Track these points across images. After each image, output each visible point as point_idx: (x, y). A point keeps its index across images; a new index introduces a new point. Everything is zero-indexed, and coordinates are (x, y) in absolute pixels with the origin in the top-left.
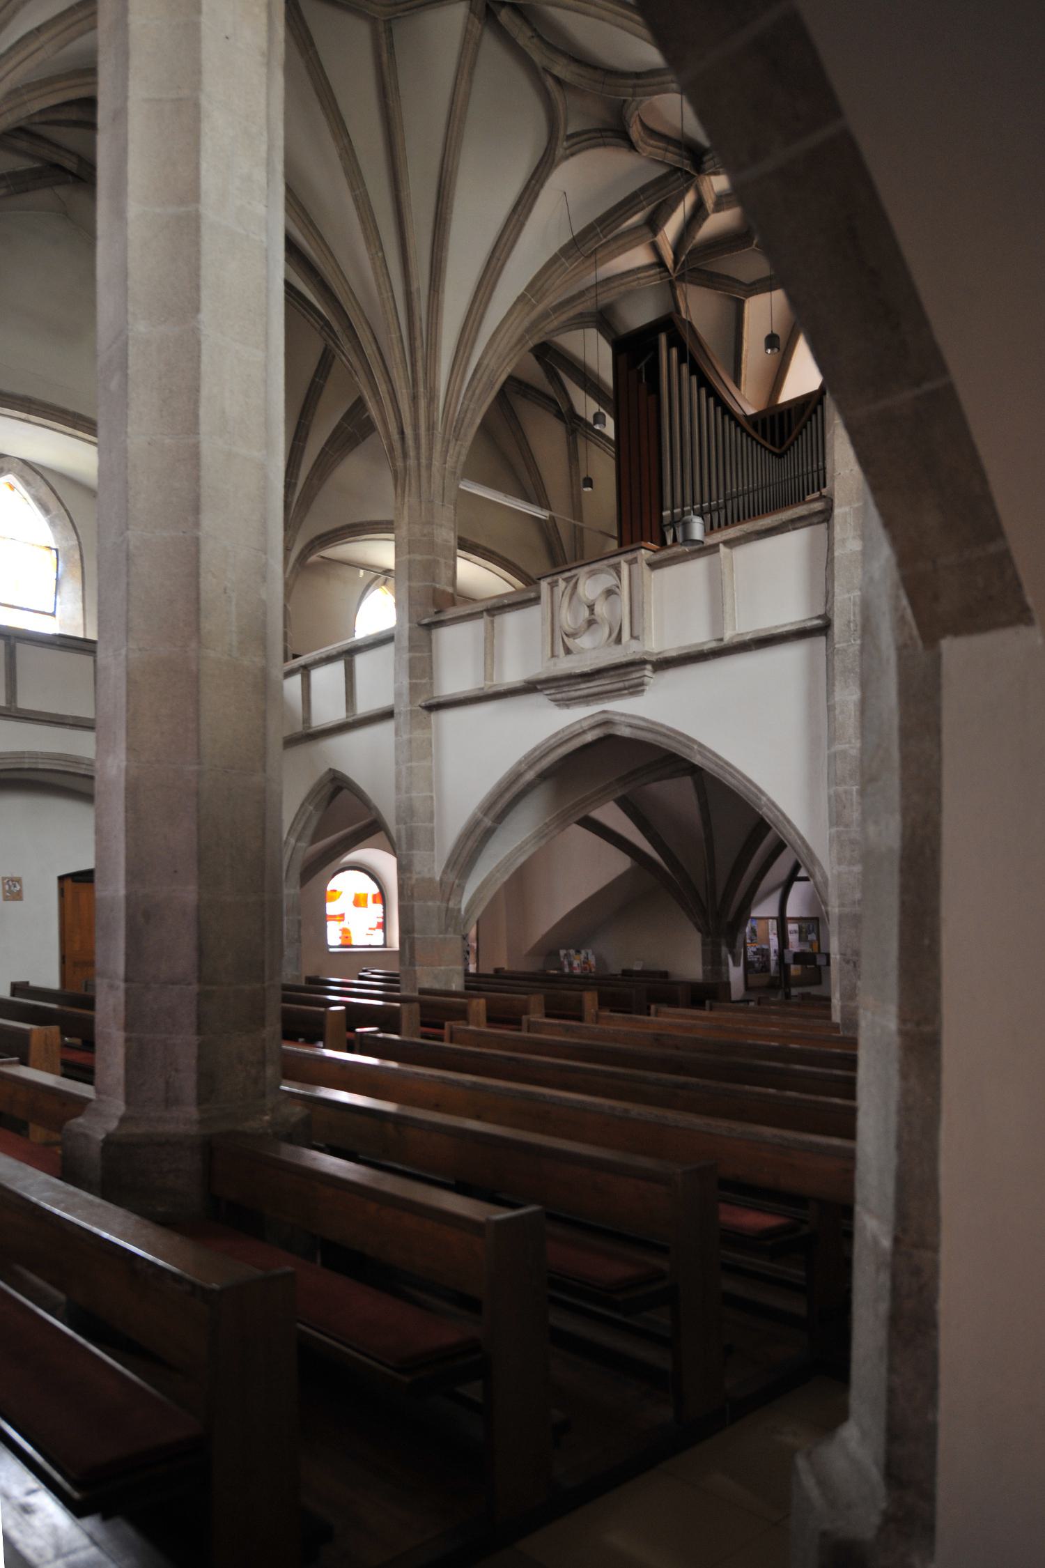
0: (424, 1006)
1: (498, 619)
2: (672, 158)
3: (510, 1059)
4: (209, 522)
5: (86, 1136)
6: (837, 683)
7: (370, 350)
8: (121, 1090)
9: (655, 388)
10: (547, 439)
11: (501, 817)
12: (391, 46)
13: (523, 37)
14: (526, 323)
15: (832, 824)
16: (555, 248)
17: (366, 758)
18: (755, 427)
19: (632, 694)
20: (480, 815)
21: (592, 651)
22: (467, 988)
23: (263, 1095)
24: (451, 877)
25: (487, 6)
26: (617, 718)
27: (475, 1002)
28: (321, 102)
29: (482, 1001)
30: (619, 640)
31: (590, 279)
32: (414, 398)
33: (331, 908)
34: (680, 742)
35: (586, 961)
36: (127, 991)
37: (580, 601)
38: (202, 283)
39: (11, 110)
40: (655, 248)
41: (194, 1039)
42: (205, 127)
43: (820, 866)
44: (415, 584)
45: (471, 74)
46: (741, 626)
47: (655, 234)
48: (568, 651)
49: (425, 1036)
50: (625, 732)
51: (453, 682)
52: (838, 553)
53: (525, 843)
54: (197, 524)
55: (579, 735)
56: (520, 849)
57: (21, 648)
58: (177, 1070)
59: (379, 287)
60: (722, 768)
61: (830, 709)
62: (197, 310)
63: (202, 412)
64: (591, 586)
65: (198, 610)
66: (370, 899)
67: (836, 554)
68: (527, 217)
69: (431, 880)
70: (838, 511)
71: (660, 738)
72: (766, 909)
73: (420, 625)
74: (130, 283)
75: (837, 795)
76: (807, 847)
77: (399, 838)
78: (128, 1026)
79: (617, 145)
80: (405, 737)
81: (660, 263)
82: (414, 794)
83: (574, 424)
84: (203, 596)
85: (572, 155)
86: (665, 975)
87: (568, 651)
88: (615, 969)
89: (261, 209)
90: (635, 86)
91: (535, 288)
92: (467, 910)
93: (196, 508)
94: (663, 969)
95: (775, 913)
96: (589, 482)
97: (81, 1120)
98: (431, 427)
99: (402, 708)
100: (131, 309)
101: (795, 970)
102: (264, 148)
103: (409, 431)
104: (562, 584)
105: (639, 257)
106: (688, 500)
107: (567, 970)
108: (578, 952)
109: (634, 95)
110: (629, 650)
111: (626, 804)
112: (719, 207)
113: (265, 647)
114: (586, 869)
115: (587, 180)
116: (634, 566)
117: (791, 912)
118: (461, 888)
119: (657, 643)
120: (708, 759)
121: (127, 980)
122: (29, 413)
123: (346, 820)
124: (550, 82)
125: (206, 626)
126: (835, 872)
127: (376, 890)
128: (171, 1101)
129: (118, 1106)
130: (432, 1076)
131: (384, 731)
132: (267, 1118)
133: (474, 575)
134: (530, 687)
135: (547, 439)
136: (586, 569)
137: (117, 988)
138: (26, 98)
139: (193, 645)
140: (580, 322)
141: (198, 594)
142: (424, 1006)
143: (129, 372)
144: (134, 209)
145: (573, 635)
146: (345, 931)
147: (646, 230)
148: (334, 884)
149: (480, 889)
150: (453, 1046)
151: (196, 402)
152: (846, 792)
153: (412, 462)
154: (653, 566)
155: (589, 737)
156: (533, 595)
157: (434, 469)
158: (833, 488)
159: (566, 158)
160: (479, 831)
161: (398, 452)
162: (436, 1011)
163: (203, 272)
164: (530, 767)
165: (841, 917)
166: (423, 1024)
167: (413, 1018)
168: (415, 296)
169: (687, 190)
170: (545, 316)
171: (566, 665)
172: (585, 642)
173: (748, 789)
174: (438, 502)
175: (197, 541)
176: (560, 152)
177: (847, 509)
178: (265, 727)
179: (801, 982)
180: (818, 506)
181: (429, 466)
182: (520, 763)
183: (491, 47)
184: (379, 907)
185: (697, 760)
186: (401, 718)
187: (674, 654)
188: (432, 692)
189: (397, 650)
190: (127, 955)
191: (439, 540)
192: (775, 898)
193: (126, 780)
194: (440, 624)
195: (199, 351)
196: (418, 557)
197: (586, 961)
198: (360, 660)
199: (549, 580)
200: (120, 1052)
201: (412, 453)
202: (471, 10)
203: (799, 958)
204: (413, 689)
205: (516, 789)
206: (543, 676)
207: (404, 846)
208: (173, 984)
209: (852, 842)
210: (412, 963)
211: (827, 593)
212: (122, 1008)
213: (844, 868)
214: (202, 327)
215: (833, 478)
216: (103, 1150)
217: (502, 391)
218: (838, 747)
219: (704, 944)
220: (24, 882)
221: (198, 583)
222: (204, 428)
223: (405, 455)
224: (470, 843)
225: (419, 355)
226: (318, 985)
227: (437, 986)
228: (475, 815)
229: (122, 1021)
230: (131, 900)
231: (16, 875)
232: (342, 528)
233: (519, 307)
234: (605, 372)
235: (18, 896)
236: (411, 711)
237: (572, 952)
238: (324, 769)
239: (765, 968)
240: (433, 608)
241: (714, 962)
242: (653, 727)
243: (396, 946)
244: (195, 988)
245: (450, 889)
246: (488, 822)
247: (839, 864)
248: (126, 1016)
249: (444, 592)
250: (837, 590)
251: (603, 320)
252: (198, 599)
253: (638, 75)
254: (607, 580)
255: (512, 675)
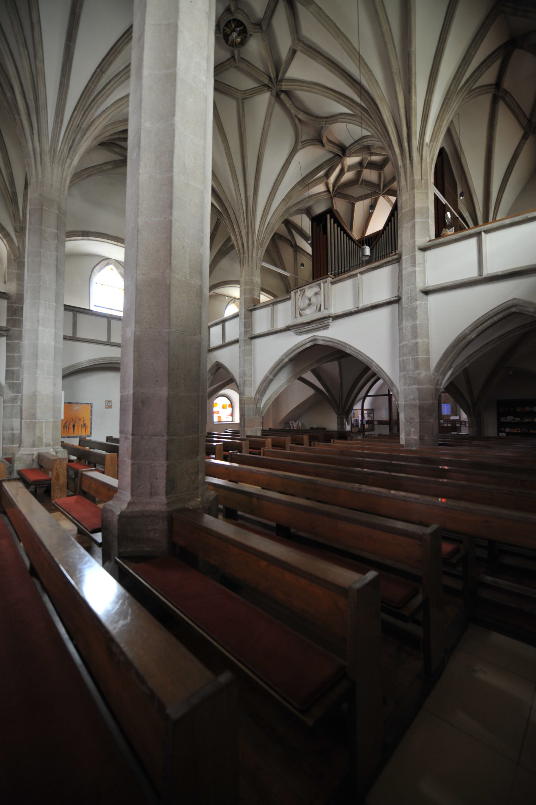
0: (251, 442)
1: (275, 306)
2: (336, 150)
3: (292, 463)
4: (176, 214)
5: (112, 511)
6: (404, 319)
7: (233, 217)
8: (129, 489)
9: (325, 232)
10: (287, 253)
11: (275, 375)
12: (243, 109)
13: (288, 103)
14: (285, 209)
15: (401, 371)
16: (295, 183)
17: (228, 358)
18: (360, 243)
19: (324, 329)
20: (268, 374)
21: (310, 314)
22: (262, 435)
23: (197, 488)
24: (258, 396)
25: (277, 93)
26: (318, 338)
27: (268, 439)
28: (219, 130)
29: (270, 439)
30: (320, 310)
31: (307, 194)
32: (247, 233)
33: (215, 409)
34: (341, 345)
35: (298, 425)
36: (133, 440)
37: (306, 297)
38: (177, 104)
39: (112, 129)
40: (327, 185)
41: (165, 463)
42: (180, 36)
43: (396, 387)
44: (247, 296)
45: (270, 118)
46: (366, 302)
47: (328, 179)
48: (301, 315)
49: (251, 453)
50: (321, 343)
51: (259, 329)
52: (404, 272)
53: (283, 384)
54: (171, 214)
55: (304, 344)
56: (281, 386)
57: (113, 322)
58: (156, 478)
59: (236, 195)
60: (358, 353)
61: (400, 330)
62: (174, 115)
63: (175, 162)
64: (310, 292)
65: (170, 255)
66: (228, 406)
67: (403, 273)
68: (287, 170)
69: (251, 398)
70: (404, 258)
71: (334, 344)
72: (358, 406)
73: (248, 310)
74: (143, 104)
75: (403, 361)
76: (390, 380)
77: (240, 383)
78: (133, 457)
79: (318, 145)
80: (243, 348)
81: (328, 191)
82: (246, 368)
83: (297, 249)
84: (173, 248)
85: (303, 148)
86: (324, 429)
87: (301, 315)
88: (308, 427)
89: (204, 78)
90: (326, 121)
91: (288, 196)
92: (263, 408)
93: (171, 206)
94: (324, 427)
95: (360, 408)
96: (302, 265)
97: (110, 502)
98: (253, 243)
99: (242, 339)
100: (143, 116)
101: (366, 426)
102: (206, 53)
103: (245, 244)
104: (299, 292)
105: (320, 188)
106: (337, 269)
107: (292, 428)
108: (296, 422)
109: (326, 124)
110: (324, 313)
111: (315, 372)
112: (349, 170)
113: (202, 276)
114: (302, 394)
115: (308, 157)
116: (326, 284)
117: (365, 407)
118: (261, 400)
119: (334, 310)
120: (353, 351)
121: (133, 435)
122: (118, 242)
123: (222, 378)
124: (297, 121)
125: (174, 262)
126: (402, 389)
127: (230, 403)
128: (153, 494)
129: (126, 497)
130: (265, 472)
131: (236, 347)
132: (199, 499)
133: (264, 298)
134: (288, 329)
135: (287, 253)
136: (308, 286)
137: (129, 439)
138: (117, 125)
139: (168, 271)
140: (300, 211)
141: (171, 246)
142: (251, 442)
143: (141, 144)
144: (146, 72)
145: (303, 310)
146: (219, 417)
147: (325, 178)
148: (216, 401)
149: (267, 401)
150: (264, 457)
151: (172, 157)
152: (407, 359)
153: (246, 255)
154: (333, 283)
155: (308, 345)
156: (288, 297)
157: (254, 257)
158: (402, 249)
159: (301, 149)
160: (268, 380)
161: (242, 252)
162: (255, 445)
163: (177, 99)
164: (286, 357)
165: (405, 406)
166: (250, 448)
167: (239, 446)
168: (248, 197)
169: (339, 162)
170: (290, 208)
171: (300, 320)
172: (307, 312)
173: (368, 361)
174: (255, 268)
175: (171, 221)
176: (299, 147)
177: (407, 256)
178: (201, 313)
179: (368, 430)
180: (396, 257)
181: (252, 256)
182: (283, 355)
183: (278, 109)
184: (231, 408)
185: (348, 351)
186: (241, 342)
187: (340, 313)
188: (252, 333)
189: (240, 319)
190: (133, 423)
191: (255, 281)
192: (360, 403)
193: (134, 337)
194: (255, 309)
195: (174, 134)
196: (248, 287)
197: (298, 425)
198: (227, 324)
199: (294, 291)
200: (130, 469)
201: (246, 252)
202: (271, 95)
203: (368, 422)
204: (246, 332)
205: (281, 365)
206: (292, 324)
207: (242, 386)
208: (155, 436)
209: (410, 377)
210: (244, 427)
211: (399, 288)
212: (130, 449)
213: (406, 387)
214: (176, 123)
215: (402, 246)
216: (119, 520)
217: (273, 238)
218: (404, 343)
219: (338, 418)
220: (113, 402)
221: (171, 242)
222: (176, 170)
223: (244, 253)
224: (264, 384)
225: (249, 218)
226: (210, 435)
227: (252, 434)
228: (267, 374)
229: (130, 455)
230: (134, 394)
231: (110, 400)
232: (221, 282)
233: (283, 202)
234: (308, 231)
235: (110, 407)
236: (245, 340)
237: (294, 422)
238: (214, 361)
239: (357, 426)
240: (251, 306)
241: (341, 424)
242: (332, 341)
243: (237, 420)
244: (165, 438)
245: (257, 401)
246: (271, 377)
247: (405, 385)
248: (132, 452)
249: (256, 299)
250: (404, 286)
251: (308, 211)
252: (171, 250)
253: (327, 118)
254: (316, 289)
255: (281, 325)
